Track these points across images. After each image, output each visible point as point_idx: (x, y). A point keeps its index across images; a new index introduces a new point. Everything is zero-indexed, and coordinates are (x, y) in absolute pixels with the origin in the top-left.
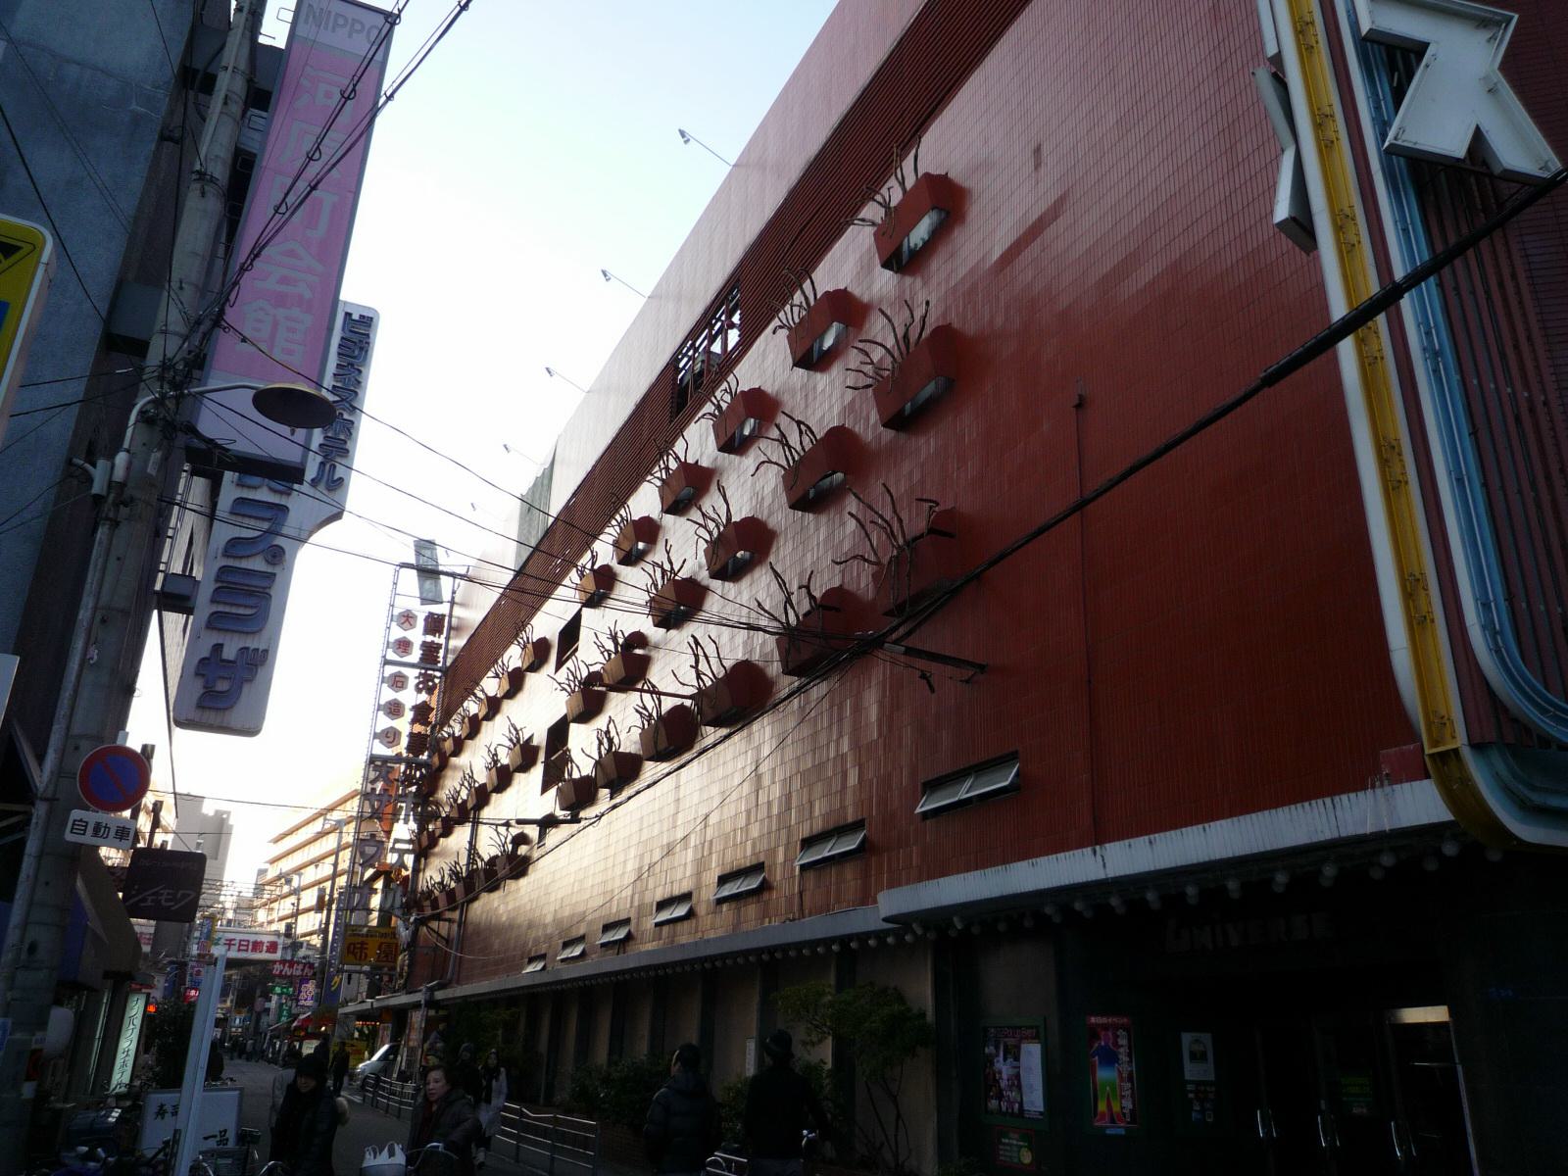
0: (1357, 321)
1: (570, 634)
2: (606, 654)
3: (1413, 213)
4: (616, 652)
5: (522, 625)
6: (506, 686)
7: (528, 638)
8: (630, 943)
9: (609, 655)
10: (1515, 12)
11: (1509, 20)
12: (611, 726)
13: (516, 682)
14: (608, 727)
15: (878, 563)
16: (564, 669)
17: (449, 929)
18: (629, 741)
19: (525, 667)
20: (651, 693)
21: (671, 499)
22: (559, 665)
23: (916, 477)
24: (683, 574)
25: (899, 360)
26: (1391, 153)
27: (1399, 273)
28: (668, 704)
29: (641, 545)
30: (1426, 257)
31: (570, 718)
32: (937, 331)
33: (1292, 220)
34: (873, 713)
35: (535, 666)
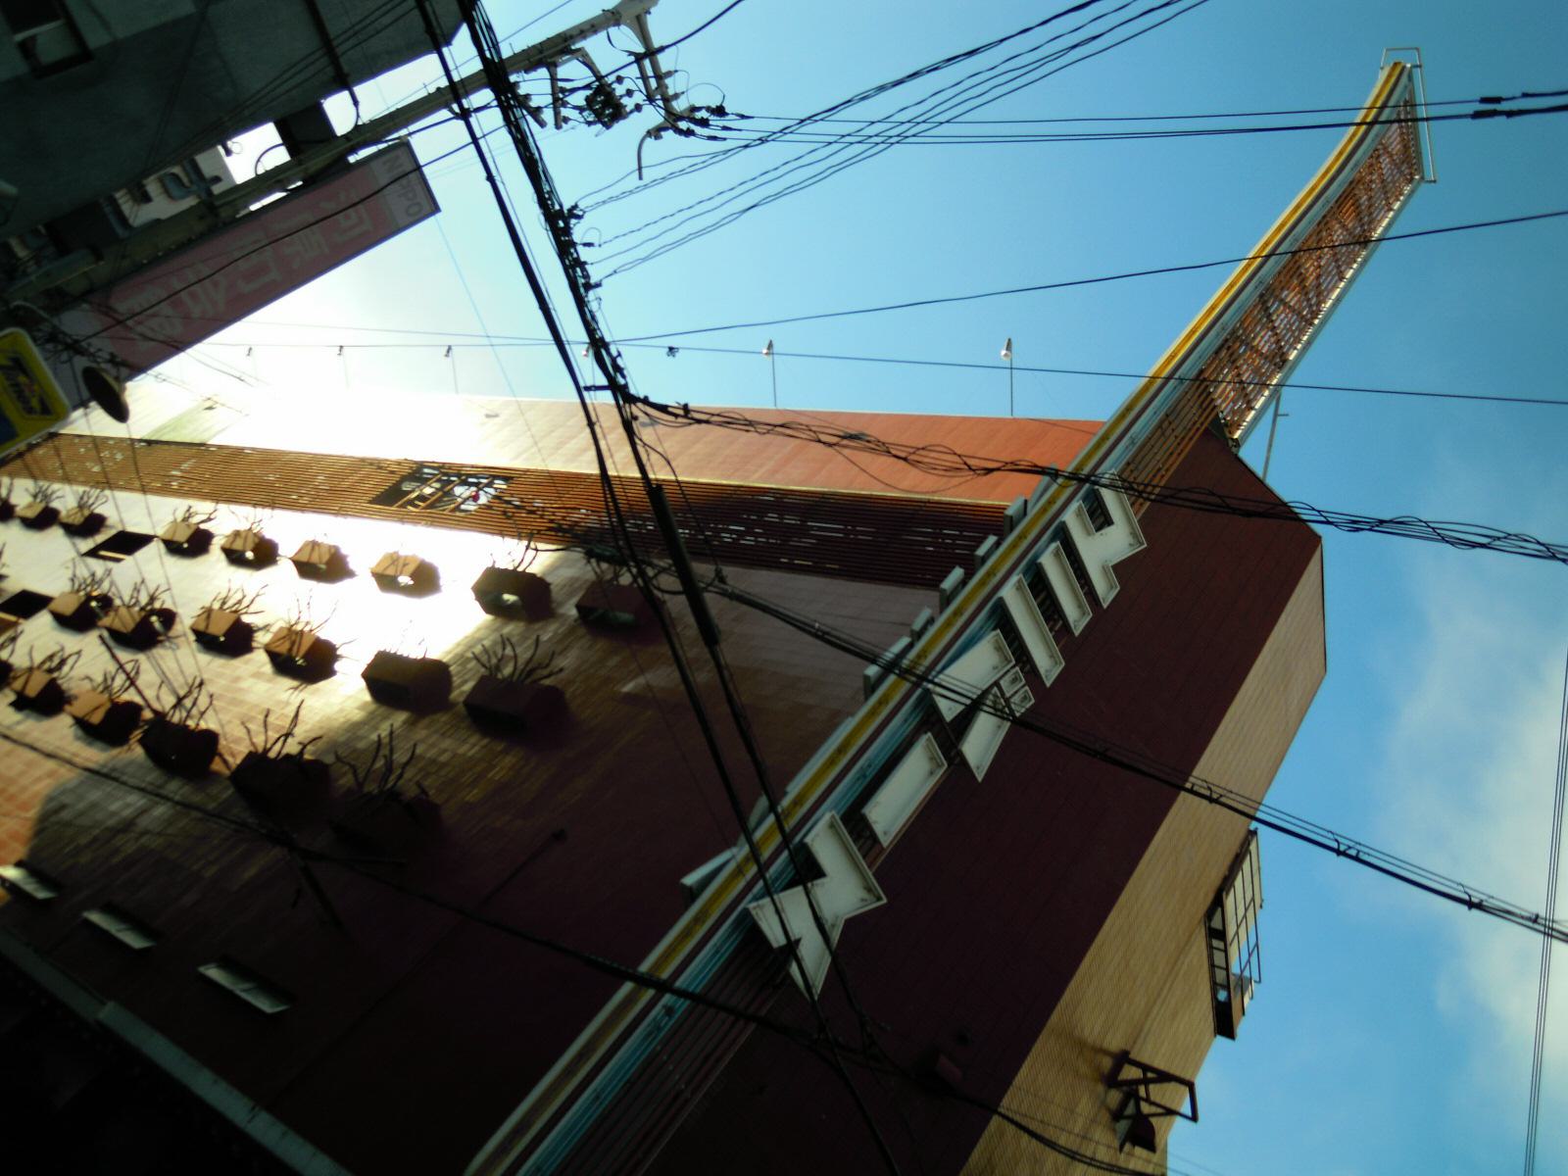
0: (644, 981)
1: (129, 543)
2: (133, 601)
3: (728, 950)
4: (142, 609)
5: (107, 482)
6: (31, 514)
7: (93, 504)
8: (65, 687)
9: (135, 605)
10: (887, 896)
11: (879, 899)
12: (74, 658)
13: (44, 519)
14: (70, 656)
15: (360, 785)
16: (92, 562)
17: (122, 197)
18: (73, 678)
19: (65, 520)
20: (128, 677)
21: (304, 558)
22: (93, 553)
23: (444, 758)
24: (246, 619)
25: (515, 678)
26: (746, 913)
27: (679, 984)
28: (130, 695)
29: (250, 555)
30: (698, 990)
31: (53, 606)
32: (551, 689)
33: (690, 889)
34: (250, 872)
35: (76, 531)
